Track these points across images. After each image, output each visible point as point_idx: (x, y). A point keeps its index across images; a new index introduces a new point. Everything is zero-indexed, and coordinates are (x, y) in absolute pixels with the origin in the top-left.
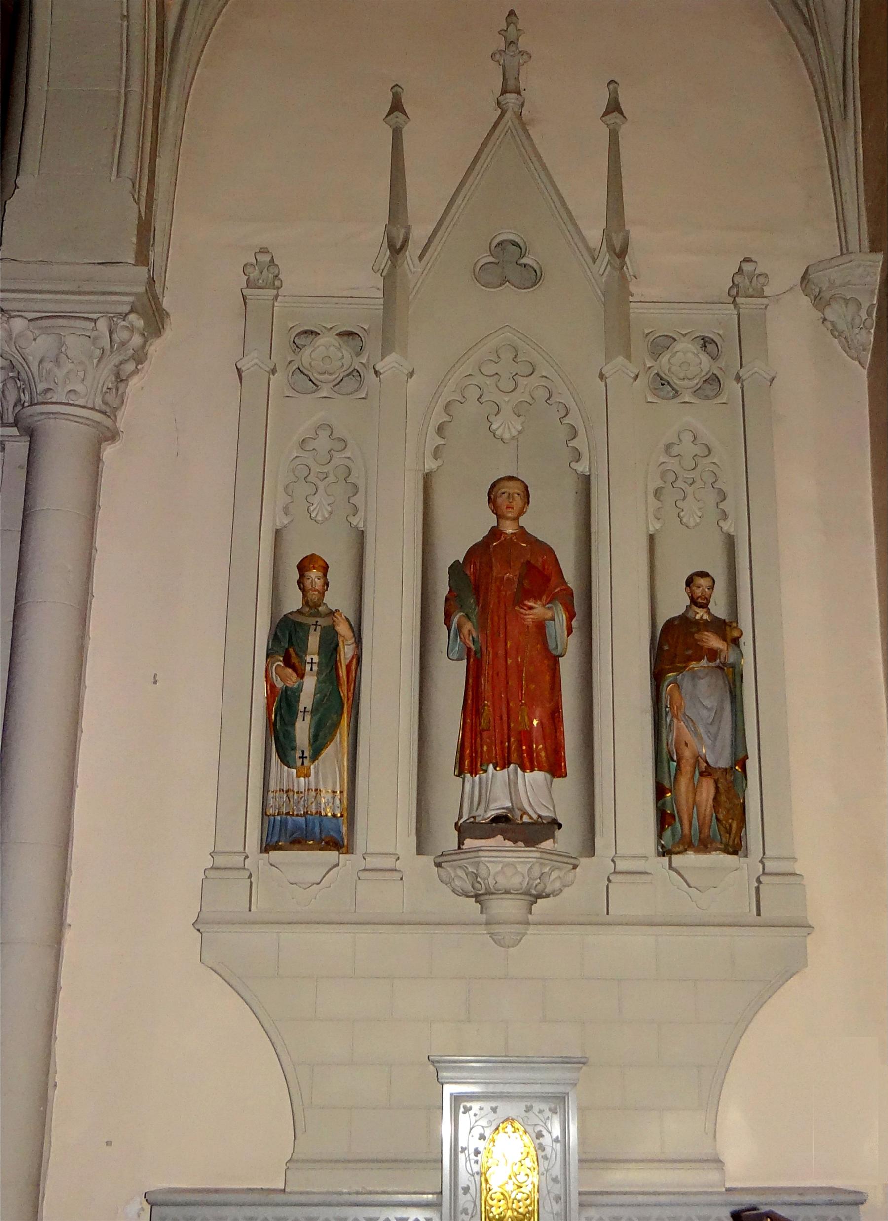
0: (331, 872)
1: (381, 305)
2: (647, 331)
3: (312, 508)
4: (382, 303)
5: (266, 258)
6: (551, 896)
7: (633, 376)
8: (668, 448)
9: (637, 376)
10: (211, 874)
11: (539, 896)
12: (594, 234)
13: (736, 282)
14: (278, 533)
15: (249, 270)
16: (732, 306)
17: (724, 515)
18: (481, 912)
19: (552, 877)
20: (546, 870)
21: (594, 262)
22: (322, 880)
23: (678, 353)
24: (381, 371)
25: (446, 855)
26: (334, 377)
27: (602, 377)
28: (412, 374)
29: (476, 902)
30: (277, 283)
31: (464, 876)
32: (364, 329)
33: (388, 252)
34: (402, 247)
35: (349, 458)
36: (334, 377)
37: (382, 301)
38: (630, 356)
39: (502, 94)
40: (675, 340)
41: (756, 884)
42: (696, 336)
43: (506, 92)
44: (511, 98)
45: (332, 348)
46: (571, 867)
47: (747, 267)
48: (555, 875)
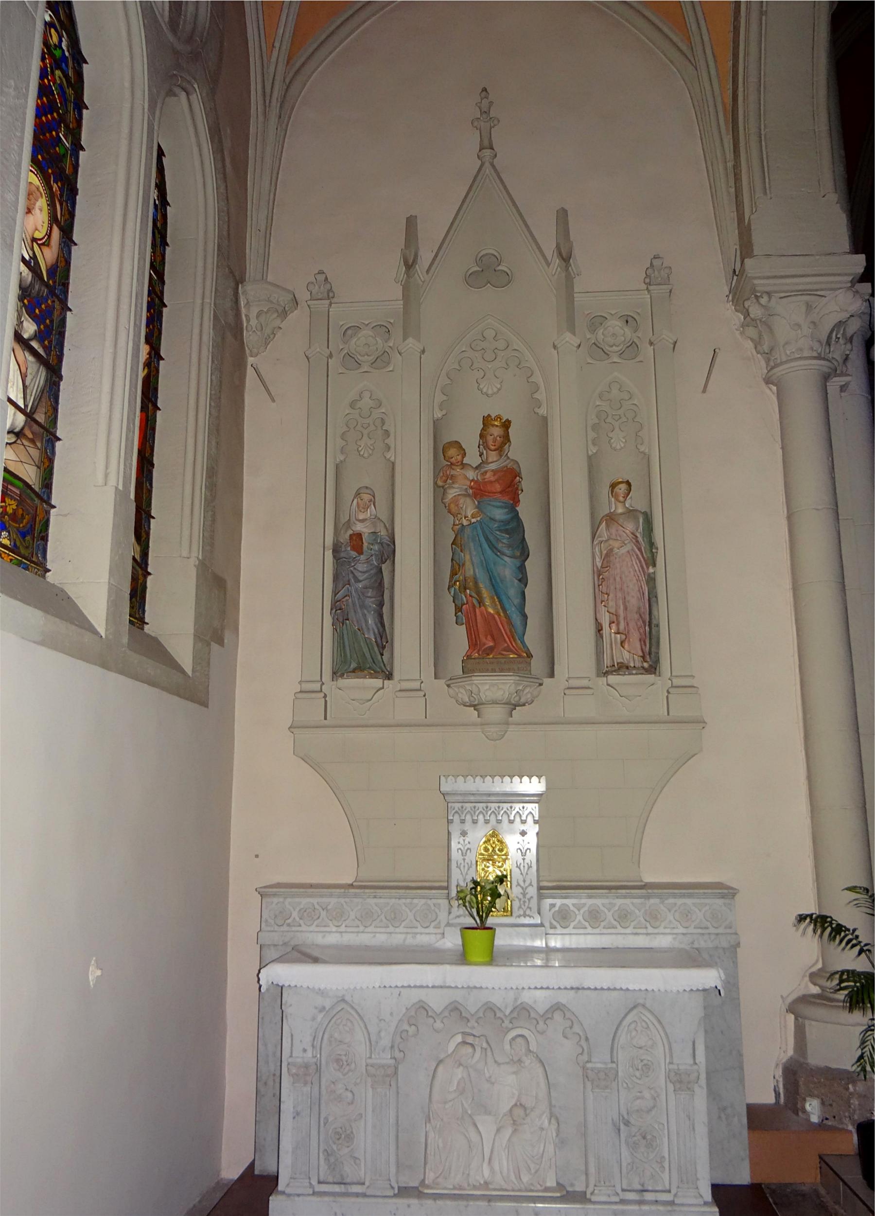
0: (379, 692)
1: (401, 305)
2: (341, 324)
3: (360, 449)
4: (402, 303)
5: (322, 277)
6: (527, 704)
7: (576, 345)
8: (352, 405)
9: (580, 345)
10: (300, 695)
11: (515, 706)
12: (549, 247)
13: (648, 274)
14: (337, 467)
15: (311, 287)
16: (646, 292)
17: (388, 448)
18: (478, 717)
19: (525, 692)
20: (521, 688)
21: (548, 267)
22: (373, 697)
23: (609, 328)
24: (403, 351)
25: (454, 679)
26: (372, 358)
27: (555, 347)
28: (423, 352)
29: (475, 709)
30: (331, 295)
31: (464, 692)
32: (390, 323)
33: (404, 268)
34: (412, 266)
35: (383, 413)
36: (372, 358)
37: (402, 302)
38: (575, 332)
39: (480, 151)
40: (607, 319)
41: (667, 694)
42: (622, 315)
43: (483, 149)
44: (487, 153)
45: (617, 328)
46: (538, 684)
47: (656, 263)
48: (527, 690)
